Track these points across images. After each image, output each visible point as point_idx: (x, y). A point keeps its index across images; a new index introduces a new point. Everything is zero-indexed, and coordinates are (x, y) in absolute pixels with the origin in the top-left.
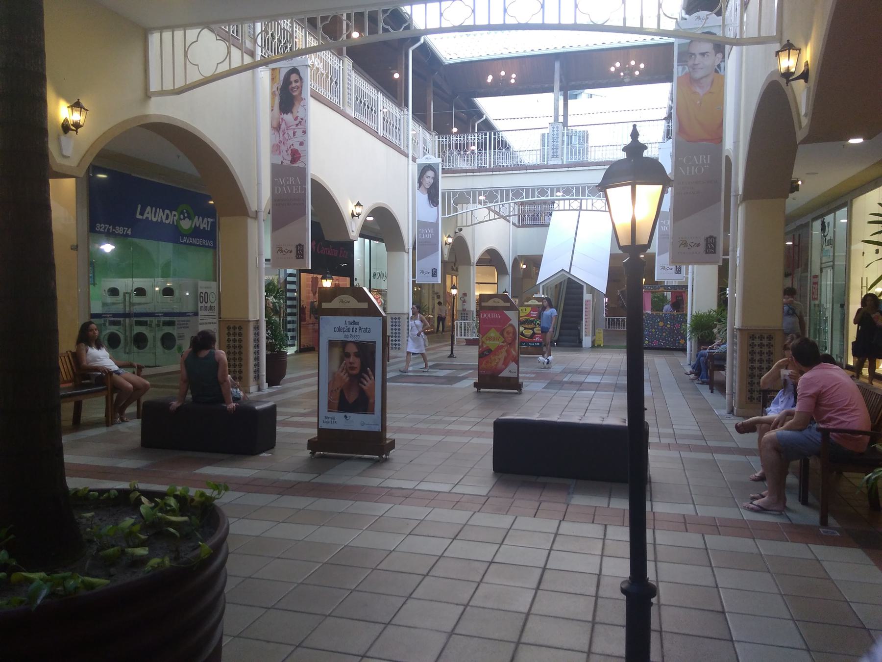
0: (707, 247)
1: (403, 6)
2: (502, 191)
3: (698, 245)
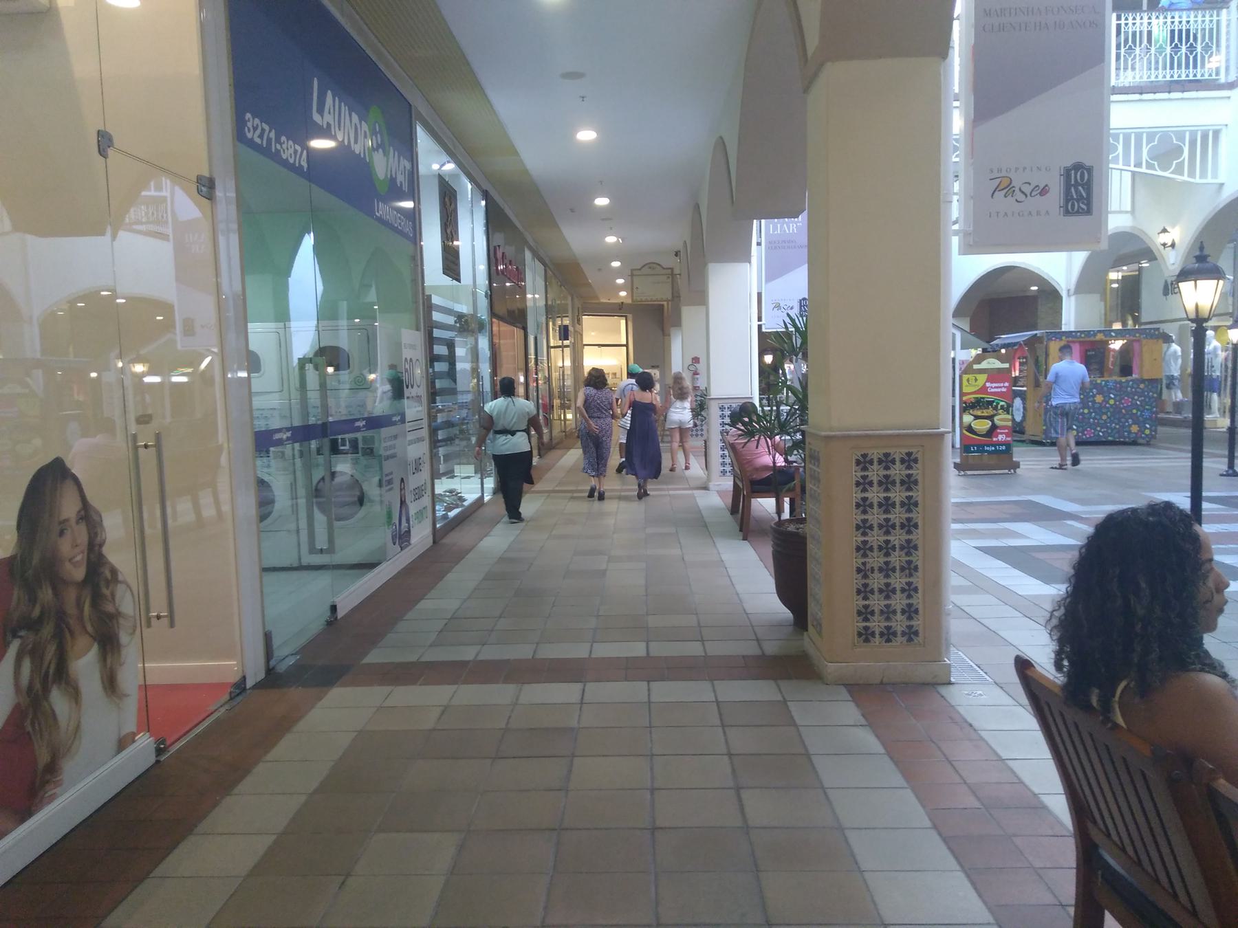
0: (1068, 198)
3: (1044, 191)
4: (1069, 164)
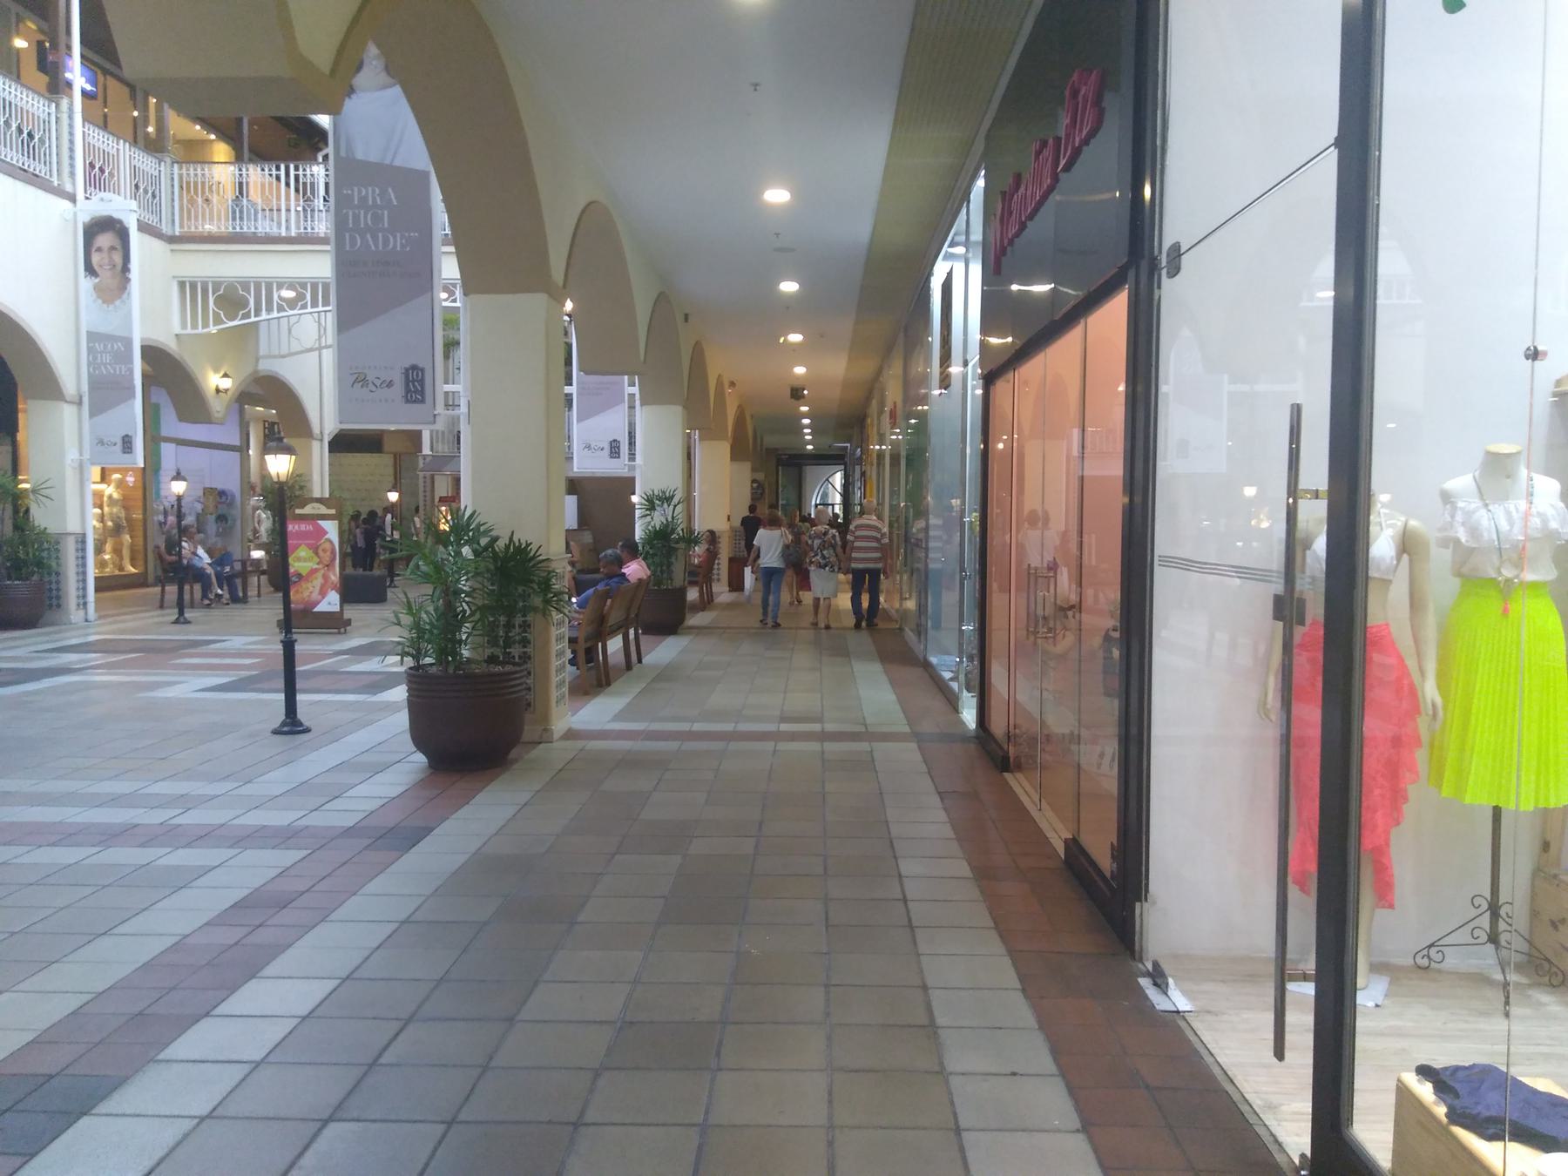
0: (408, 391)
1: (395, 71)
2: (314, 287)
3: (390, 384)
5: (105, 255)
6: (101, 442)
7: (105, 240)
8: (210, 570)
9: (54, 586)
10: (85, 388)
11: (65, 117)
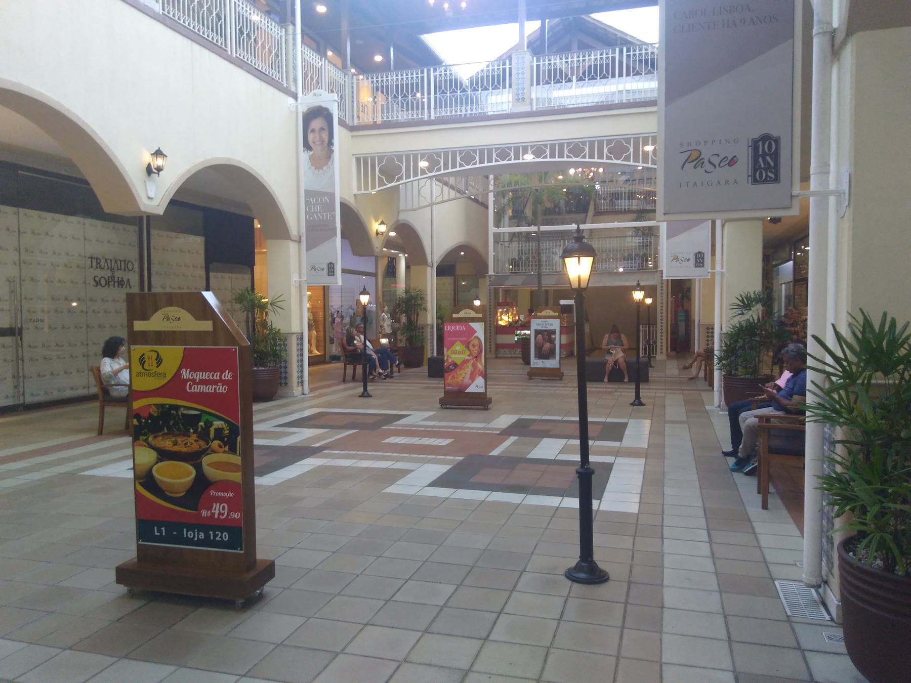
0: (756, 167)
3: (732, 162)
4: (756, 136)
5: (317, 134)
6: (314, 268)
7: (317, 124)
8: (375, 356)
9: (283, 370)
10: (303, 231)
11: (291, 37)
